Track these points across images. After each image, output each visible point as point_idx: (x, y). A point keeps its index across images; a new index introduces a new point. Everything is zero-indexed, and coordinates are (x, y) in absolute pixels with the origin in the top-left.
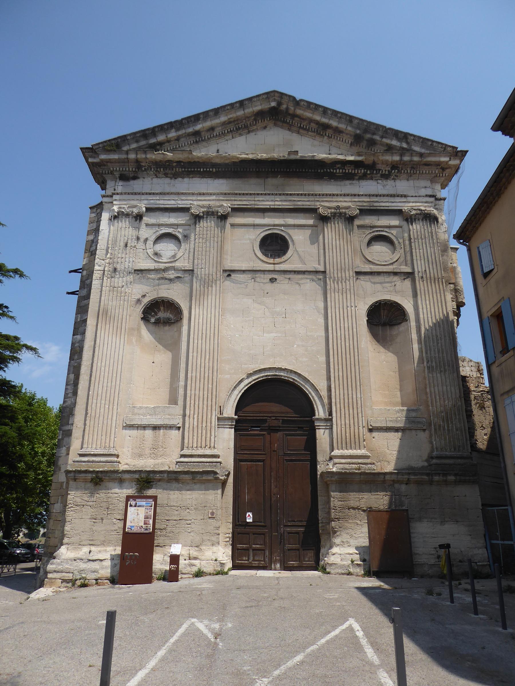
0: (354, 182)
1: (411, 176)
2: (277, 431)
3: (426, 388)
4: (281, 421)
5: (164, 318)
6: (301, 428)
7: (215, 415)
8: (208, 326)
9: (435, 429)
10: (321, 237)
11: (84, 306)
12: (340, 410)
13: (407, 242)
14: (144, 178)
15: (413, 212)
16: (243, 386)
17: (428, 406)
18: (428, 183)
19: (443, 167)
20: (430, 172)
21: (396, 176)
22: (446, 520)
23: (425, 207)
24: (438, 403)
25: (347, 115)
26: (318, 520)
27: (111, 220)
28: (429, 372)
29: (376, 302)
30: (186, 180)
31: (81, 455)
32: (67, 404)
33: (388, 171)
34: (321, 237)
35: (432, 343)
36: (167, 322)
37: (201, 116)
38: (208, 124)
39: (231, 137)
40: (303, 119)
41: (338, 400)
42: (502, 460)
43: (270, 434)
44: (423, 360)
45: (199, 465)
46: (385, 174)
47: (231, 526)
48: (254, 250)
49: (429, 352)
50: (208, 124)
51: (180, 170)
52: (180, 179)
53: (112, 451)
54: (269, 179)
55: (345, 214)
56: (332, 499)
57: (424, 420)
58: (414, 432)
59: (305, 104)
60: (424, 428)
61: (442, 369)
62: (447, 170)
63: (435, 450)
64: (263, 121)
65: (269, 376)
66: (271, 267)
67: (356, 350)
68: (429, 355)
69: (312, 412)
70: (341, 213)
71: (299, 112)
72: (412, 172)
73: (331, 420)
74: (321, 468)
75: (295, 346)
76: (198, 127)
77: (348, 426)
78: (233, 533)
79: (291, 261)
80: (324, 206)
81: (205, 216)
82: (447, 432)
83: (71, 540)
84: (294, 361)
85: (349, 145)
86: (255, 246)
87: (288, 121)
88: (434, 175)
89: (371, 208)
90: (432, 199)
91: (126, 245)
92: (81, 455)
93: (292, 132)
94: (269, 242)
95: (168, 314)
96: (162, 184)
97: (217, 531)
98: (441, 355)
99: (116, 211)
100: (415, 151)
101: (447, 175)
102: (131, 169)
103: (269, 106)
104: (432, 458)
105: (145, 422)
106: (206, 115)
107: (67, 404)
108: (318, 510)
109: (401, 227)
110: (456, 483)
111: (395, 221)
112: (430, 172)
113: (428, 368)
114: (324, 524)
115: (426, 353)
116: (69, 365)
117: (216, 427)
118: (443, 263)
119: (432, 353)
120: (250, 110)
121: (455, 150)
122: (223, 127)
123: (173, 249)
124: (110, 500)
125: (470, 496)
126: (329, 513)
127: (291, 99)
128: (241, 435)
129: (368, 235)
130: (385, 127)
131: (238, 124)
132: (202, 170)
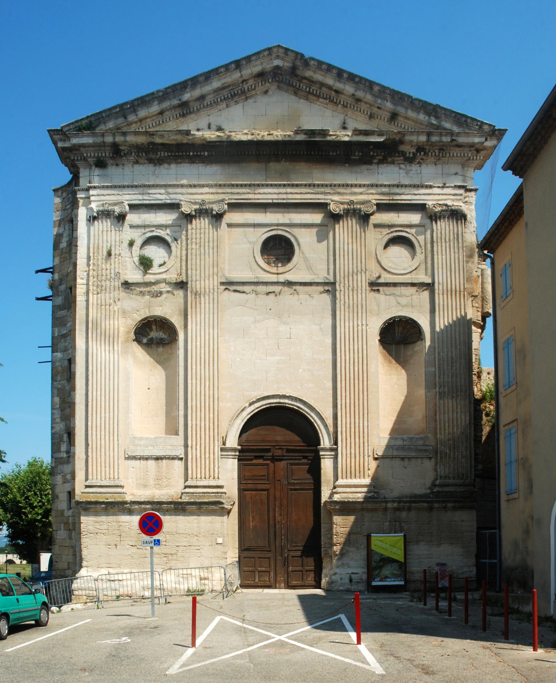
0: (372, 167)
1: (439, 159)
2: (281, 460)
3: (436, 415)
4: (285, 450)
5: (157, 338)
6: (305, 457)
7: (218, 445)
8: (207, 349)
9: (441, 458)
10: (331, 234)
11: (61, 318)
12: (346, 439)
13: (429, 246)
14: (123, 165)
15: (438, 209)
16: (246, 415)
17: (437, 433)
18: (458, 169)
19: (478, 149)
20: (462, 155)
21: (421, 159)
22: (442, 542)
23: (453, 200)
24: (447, 431)
25: (366, 80)
26: (321, 545)
27: (90, 221)
28: (440, 398)
29: (390, 319)
30: (173, 166)
31: (87, 487)
32: (55, 430)
33: (413, 153)
34: (331, 234)
35: (446, 367)
36: (161, 343)
37: (189, 83)
38: (197, 93)
39: (224, 105)
40: (312, 82)
41: (344, 429)
42: (497, 489)
43: (273, 463)
44: (435, 384)
45: (205, 496)
46: (409, 157)
47: (237, 551)
48: (254, 257)
49: (442, 376)
50: (197, 93)
51: (166, 154)
52: (166, 166)
53: (117, 483)
54: (271, 164)
55: (360, 210)
56: (335, 526)
57: (431, 448)
58: (419, 460)
59: (315, 63)
60: (431, 456)
61: (454, 395)
62: (482, 152)
63: (439, 478)
64: (263, 83)
65: (273, 403)
66: (274, 278)
67: (365, 375)
68: (442, 380)
69: (317, 441)
70: (354, 210)
71: (308, 74)
72: (441, 155)
73: (336, 450)
74: (325, 496)
75: (301, 370)
76: (187, 96)
77: (353, 455)
78: (239, 557)
79: (295, 271)
80: (336, 201)
81: (197, 215)
82: (452, 459)
83: (89, 563)
84: (299, 387)
85: (367, 117)
86: (255, 251)
87: (294, 84)
88: (466, 159)
89: (391, 202)
90: (461, 191)
91: (109, 254)
92: (87, 487)
93: (300, 98)
94: (271, 244)
95: (161, 334)
96: (144, 173)
97: (224, 556)
98: (454, 380)
99: (95, 210)
100: (445, 129)
101: (482, 158)
102: (107, 155)
103: (271, 66)
104: (435, 486)
105: (147, 453)
106: (194, 82)
107: (55, 430)
108: (320, 536)
109: (424, 226)
110: (455, 509)
111: (415, 218)
112: (462, 155)
113: (440, 393)
114: (326, 549)
115: (439, 377)
116: (52, 387)
117: (220, 457)
118: (467, 271)
119: (446, 377)
120: (248, 71)
121: (492, 128)
122: (215, 94)
123: (161, 255)
124: (121, 528)
125: (466, 520)
126: (331, 538)
127: (299, 57)
128: (245, 465)
129: (386, 235)
130: (411, 97)
131: (234, 89)
132: (191, 154)
